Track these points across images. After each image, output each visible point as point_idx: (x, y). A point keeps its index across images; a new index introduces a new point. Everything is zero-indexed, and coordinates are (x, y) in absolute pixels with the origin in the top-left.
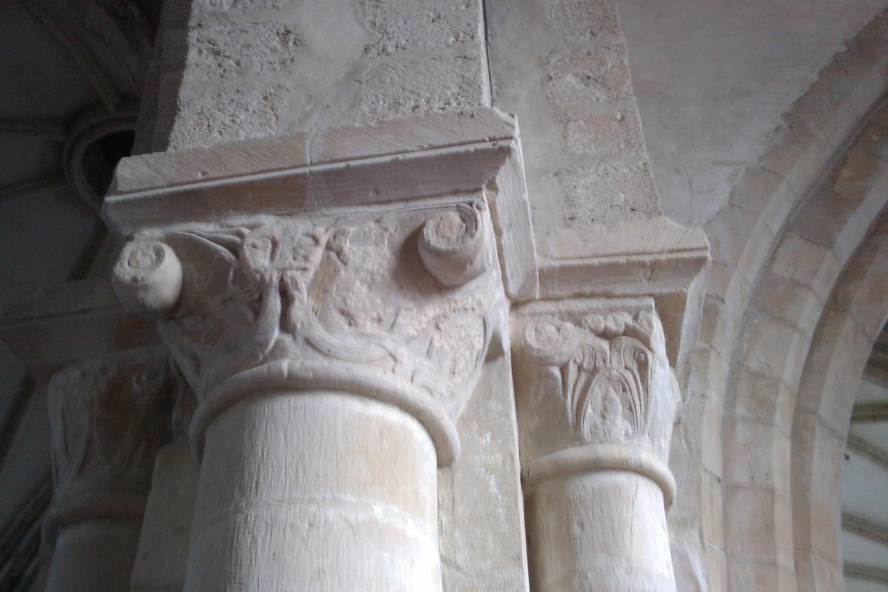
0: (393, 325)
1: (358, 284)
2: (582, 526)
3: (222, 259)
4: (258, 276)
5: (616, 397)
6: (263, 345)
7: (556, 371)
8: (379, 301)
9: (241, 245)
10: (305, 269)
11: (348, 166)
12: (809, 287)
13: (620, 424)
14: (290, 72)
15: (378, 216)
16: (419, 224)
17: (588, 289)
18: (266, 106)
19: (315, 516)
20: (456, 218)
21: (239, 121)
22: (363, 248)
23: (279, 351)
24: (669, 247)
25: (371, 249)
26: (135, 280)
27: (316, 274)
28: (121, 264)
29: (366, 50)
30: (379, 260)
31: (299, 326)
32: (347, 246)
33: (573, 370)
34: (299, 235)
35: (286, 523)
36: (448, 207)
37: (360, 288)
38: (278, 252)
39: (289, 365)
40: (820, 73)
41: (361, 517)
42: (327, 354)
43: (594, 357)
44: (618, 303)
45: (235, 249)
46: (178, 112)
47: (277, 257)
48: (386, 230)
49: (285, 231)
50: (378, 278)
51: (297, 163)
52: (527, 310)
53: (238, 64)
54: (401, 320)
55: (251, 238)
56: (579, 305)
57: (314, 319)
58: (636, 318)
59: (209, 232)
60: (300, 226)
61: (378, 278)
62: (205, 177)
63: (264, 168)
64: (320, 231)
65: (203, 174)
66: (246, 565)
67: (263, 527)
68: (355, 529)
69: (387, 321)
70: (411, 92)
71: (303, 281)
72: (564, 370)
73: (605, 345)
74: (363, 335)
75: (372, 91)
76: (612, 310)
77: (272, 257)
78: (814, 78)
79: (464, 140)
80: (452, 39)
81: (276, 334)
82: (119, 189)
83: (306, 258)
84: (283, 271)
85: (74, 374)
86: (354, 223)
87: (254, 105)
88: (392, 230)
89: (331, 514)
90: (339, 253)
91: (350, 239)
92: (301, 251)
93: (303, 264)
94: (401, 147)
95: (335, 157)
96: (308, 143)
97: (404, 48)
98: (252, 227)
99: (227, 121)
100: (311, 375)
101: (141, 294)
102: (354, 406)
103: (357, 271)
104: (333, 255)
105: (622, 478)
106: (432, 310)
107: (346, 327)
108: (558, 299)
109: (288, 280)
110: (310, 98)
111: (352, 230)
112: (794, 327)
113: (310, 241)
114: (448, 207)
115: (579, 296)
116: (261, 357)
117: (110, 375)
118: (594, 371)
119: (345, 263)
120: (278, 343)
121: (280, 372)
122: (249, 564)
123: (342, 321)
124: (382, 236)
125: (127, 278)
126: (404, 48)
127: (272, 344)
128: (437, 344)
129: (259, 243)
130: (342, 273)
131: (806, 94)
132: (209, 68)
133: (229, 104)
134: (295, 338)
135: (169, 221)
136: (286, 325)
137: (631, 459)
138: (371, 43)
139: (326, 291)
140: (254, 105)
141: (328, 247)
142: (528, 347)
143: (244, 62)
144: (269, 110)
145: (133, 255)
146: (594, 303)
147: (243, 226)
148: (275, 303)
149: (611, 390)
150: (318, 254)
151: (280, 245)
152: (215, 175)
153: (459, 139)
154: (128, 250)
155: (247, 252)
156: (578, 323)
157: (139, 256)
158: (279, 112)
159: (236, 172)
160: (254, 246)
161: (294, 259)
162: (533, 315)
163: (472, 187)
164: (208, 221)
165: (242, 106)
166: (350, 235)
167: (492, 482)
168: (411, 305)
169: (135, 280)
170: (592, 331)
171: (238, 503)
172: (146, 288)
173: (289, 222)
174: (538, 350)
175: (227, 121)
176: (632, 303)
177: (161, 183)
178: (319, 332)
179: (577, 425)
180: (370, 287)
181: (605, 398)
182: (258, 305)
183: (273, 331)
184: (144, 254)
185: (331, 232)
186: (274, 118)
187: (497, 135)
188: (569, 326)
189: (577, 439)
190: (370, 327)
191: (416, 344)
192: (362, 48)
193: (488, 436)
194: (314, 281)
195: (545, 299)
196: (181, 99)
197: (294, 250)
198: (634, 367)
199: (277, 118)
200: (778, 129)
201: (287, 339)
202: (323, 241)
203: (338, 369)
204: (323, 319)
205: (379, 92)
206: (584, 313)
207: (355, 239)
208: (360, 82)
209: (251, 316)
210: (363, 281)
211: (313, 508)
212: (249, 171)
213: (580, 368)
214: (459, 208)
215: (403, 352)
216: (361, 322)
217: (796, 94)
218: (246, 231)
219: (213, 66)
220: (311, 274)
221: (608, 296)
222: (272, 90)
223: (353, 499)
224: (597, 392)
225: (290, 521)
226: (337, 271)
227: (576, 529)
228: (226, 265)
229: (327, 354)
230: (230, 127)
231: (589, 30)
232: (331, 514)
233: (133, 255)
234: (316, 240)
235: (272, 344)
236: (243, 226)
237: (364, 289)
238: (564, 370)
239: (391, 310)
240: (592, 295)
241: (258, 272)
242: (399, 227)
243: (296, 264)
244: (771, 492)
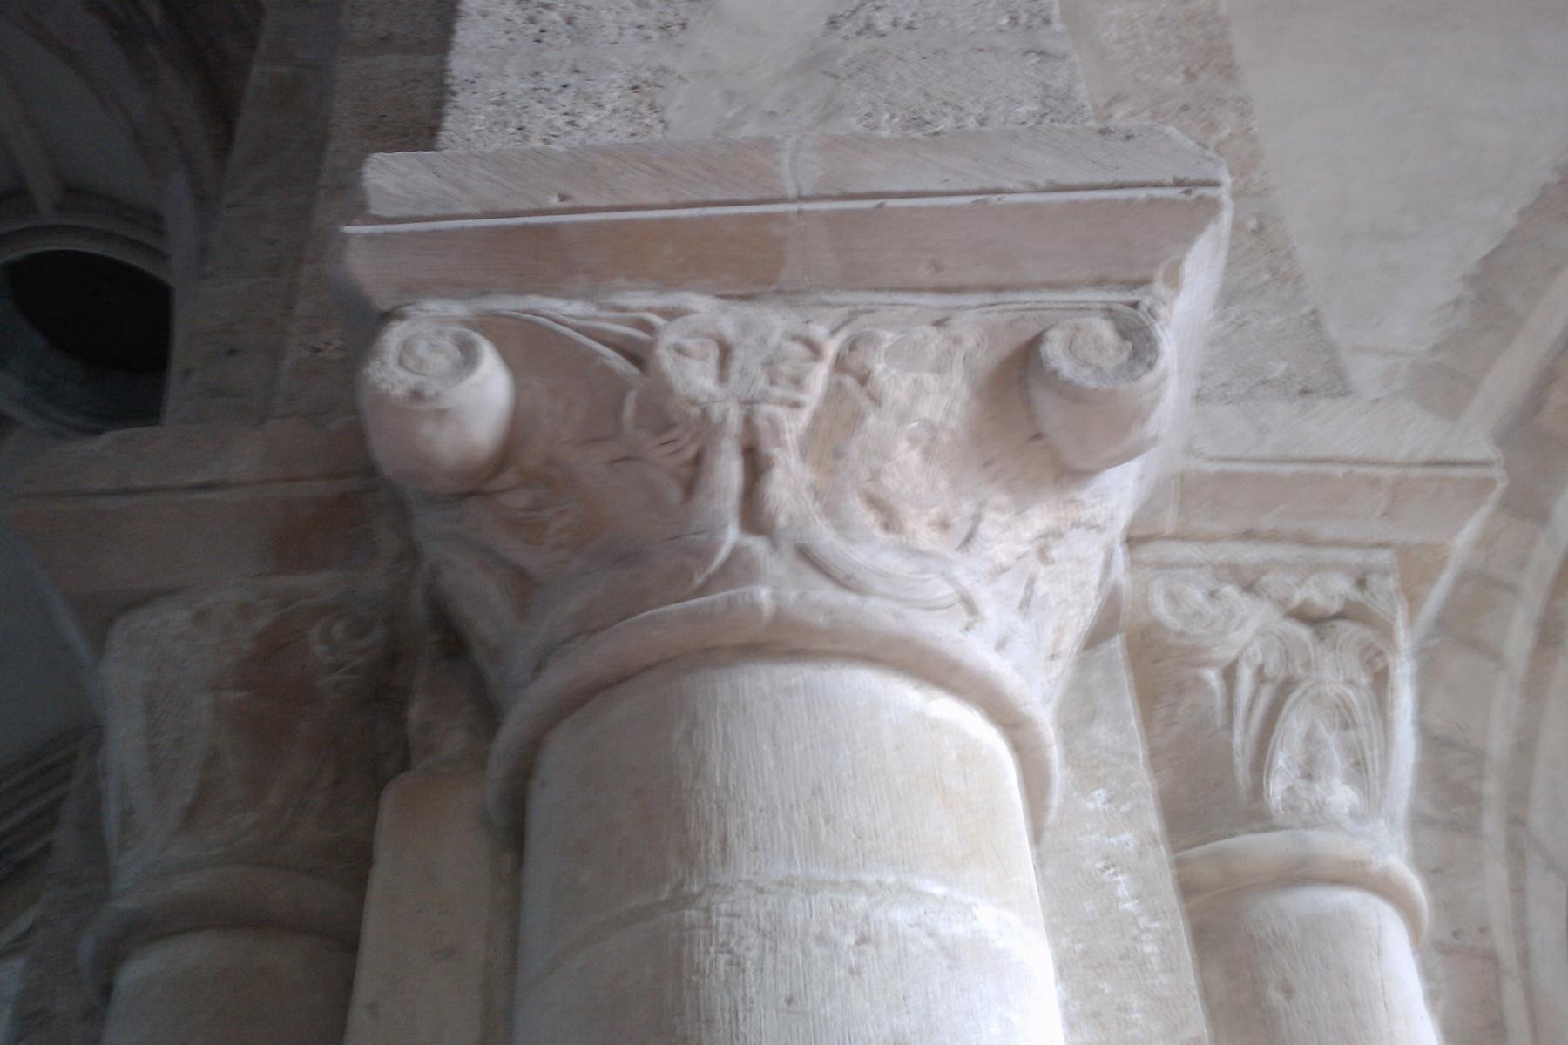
0: (969, 539)
1: (903, 445)
2: (1288, 991)
3: (608, 371)
4: (695, 411)
5: (1330, 737)
6: (704, 554)
7: (1212, 676)
8: (943, 484)
9: (651, 346)
10: (796, 405)
11: (880, 206)
12: (1514, 589)
13: (1341, 795)
14: (681, 46)
15: (938, 315)
16: (1029, 336)
17: (1267, 523)
18: (640, 103)
19: (866, 918)
20: (1105, 331)
21: (584, 124)
22: (913, 375)
23: (739, 568)
24: (1422, 457)
25: (929, 379)
26: (417, 395)
27: (816, 418)
28: (383, 363)
29: (833, 23)
30: (946, 400)
31: (782, 520)
32: (879, 367)
33: (1246, 676)
34: (775, 339)
35: (806, 934)
36: (1085, 309)
37: (907, 456)
38: (736, 366)
39: (775, 596)
40: (1521, 213)
41: (959, 929)
42: (845, 582)
43: (1287, 656)
44: (1329, 554)
45: (638, 356)
46: (448, 97)
47: (734, 377)
48: (957, 341)
49: (745, 327)
50: (945, 437)
51: (766, 194)
52: (1148, 553)
53: (570, 20)
54: (985, 529)
55: (670, 335)
56: (1250, 554)
57: (814, 508)
58: (1361, 583)
59: (570, 316)
60: (776, 322)
61: (945, 437)
62: (566, 204)
63: (697, 198)
64: (819, 331)
65: (563, 198)
66: (724, 1022)
67: (753, 938)
68: (951, 953)
69: (962, 529)
70: (946, 104)
71: (794, 426)
72: (1229, 674)
73: (1304, 633)
74: (914, 552)
75: (863, 94)
76: (1317, 568)
77: (722, 378)
78: (1510, 220)
79: (1121, 179)
80: (1004, 21)
81: (732, 535)
82: (373, 212)
83: (797, 382)
84: (749, 404)
85: (174, 617)
86: (890, 325)
87: (612, 98)
88: (970, 342)
89: (901, 916)
90: (863, 379)
91: (886, 354)
92: (785, 368)
93: (791, 394)
94: (990, 183)
95: (850, 190)
96: (785, 158)
97: (909, 27)
98: (671, 314)
99: (560, 122)
100: (821, 620)
101: (428, 429)
102: (907, 695)
103: (903, 418)
104: (850, 382)
105: (1351, 898)
106: (1039, 519)
107: (878, 532)
108: (1211, 539)
109: (761, 422)
110: (730, 96)
111: (889, 337)
112: (1495, 655)
113: (799, 349)
114: (1085, 309)
115: (1248, 535)
116: (699, 580)
117: (261, 623)
118: (1286, 686)
119: (876, 400)
120: (737, 551)
121: (755, 607)
122: (730, 1020)
123: (867, 518)
124: (950, 354)
125: (399, 391)
126: (909, 27)
127: (723, 554)
128: (1042, 588)
129: (691, 344)
130: (872, 420)
131: (1500, 248)
132: (509, 23)
133: (559, 92)
134: (775, 546)
135: (483, 291)
136: (754, 515)
137: (1371, 862)
138: (840, 12)
139: (838, 454)
140: (612, 98)
141: (840, 365)
142: (1157, 625)
143: (582, 18)
144: (644, 109)
145: (407, 347)
146: (1277, 552)
147: (649, 310)
148: (729, 470)
149: (1322, 727)
150: (819, 377)
151: (739, 354)
152: (589, 201)
153: (1110, 178)
154: (394, 336)
155: (666, 359)
156: (1249, 588)
157: (422, 349)
158: (669, 115)
159: (632, 201)
160: (680, 350)
161: (772, 382)
162: (1162, 565)
163: (1136, 275)
164: (570, 297)
165: (587, 98)
166: (885, 346)
167: (1122, 890)
168: (1003, 499)
169: (417, 395)
170: (1281, 603)
171: (680, 885)
172: (441, 414)
173: (749, 311)
174: (1181, 634)
175: (560, 122)
176: (1354, 557)
177: (469, 209)
178: (825, 537)
179: (1258, 790)
180: (927, 454)
181: (1309, 737)
182: (694, 474)
183: (725, 526)
184: (433, 347)
185: (843, 335)
186: (660, 126)
187: (1192, 176)
188: (1230, 591)
189: (1258, 817)
190: (925, 537)
191: (1004, 582)
192: (823, 20)
193: (1100, 794)
194: (812, 430)
195: (1182, 537)
196: (455, 73)
197: (769, 364)
198: (1364, 680)
199: (666, 127)
200: (1457, 302)
201: (758, 545)
202: (831, 348)
203: (880, 612)
204: (832, 511)
205: (878, 96)
206: (1261, 570)
207: (894, 354)
208: (836, 77)
209: (675, 493)
210: (914, 441)
211: (860, 902)
212: (665, 200)
213: (1260, 676)
214: (1109, 312)
215: (985, 596)
216: (910, 525)
217: (1482, 247)
218: (657, 320)
219: (519, 20)
220: (805, 416)
221: (1306, 540)
222: (647, 75)
223: (939, 890)
224: (1294, 724)
225: (815, 928)
226: (859, 417)
227: (1275, 996)
228: (620, 387)
229: (845, 582)
230: (569, 133)
231: (1182, 67)
232: (901, 916)
233: (407, 347)
234: (815, 350)
235: (723, 554)
236: (649, 310)
237: (915, 457)
238: (1229, 674)
239: (967, 507)
240: (1273, 537)
241: (694, 402)
242: (986, 338)
243: (777, 392)
244: (1491, 958)
